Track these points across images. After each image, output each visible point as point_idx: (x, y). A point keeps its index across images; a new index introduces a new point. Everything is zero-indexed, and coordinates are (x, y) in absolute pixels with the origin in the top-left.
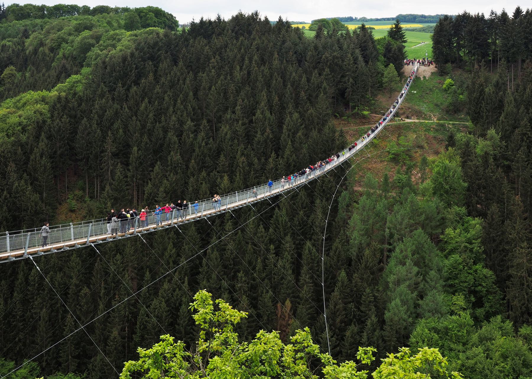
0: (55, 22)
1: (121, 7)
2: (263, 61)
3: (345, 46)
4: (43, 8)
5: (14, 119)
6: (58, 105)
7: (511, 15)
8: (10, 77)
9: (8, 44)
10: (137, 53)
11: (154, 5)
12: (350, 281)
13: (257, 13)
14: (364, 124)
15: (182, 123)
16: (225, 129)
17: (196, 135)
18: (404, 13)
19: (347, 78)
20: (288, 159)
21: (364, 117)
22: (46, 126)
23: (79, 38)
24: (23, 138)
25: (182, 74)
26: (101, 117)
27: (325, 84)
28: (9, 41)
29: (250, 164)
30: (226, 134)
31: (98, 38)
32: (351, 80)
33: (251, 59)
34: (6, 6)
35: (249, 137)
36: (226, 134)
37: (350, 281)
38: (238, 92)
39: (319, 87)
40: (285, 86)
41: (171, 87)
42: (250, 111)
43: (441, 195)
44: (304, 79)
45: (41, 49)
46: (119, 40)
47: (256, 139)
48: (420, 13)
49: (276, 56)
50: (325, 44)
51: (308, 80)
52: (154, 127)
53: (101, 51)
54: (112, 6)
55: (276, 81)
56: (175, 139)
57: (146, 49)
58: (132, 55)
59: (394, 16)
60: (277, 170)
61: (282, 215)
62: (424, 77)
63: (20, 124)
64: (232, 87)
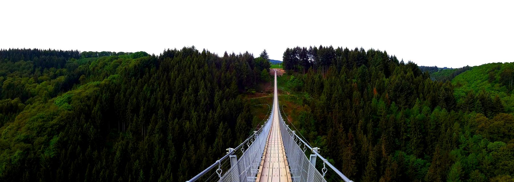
0: (101, 58)
1: (129, 52)
2: (199, 68)
4: (97, 52)
5: (84, 94)
6: (105, 88)
7: (318, 48)
8: (83, 80)
9: (82, 67)
13: (193, 47)
14: (253, 97)
15: (163, 96)
16: (184, 99)
17: (171, 102)
21: (253, 94)
22: (99, 97)
23: (112, 63)
24: (88, 103)
25: (162, 73)
28: (82, 66)
29: (199, 116)
30: (186, 101)
31: (121, 62)
33: (194, 66)
34: (81, 52)
35: (197, 103)
38: (189, 82)
41: (158, 79)
42: (196, 91)
45: (96, 68)
46: (130, 62)
49: (206, 65)
52: (151, 98)
53: (122, 67)
54: (125, 52)
56: (161, 103)
57: (144, 63)
58: (139, 65)
61: (283, 88)
62: (280, 76)
63: (87, 96)
64: (186, 79)
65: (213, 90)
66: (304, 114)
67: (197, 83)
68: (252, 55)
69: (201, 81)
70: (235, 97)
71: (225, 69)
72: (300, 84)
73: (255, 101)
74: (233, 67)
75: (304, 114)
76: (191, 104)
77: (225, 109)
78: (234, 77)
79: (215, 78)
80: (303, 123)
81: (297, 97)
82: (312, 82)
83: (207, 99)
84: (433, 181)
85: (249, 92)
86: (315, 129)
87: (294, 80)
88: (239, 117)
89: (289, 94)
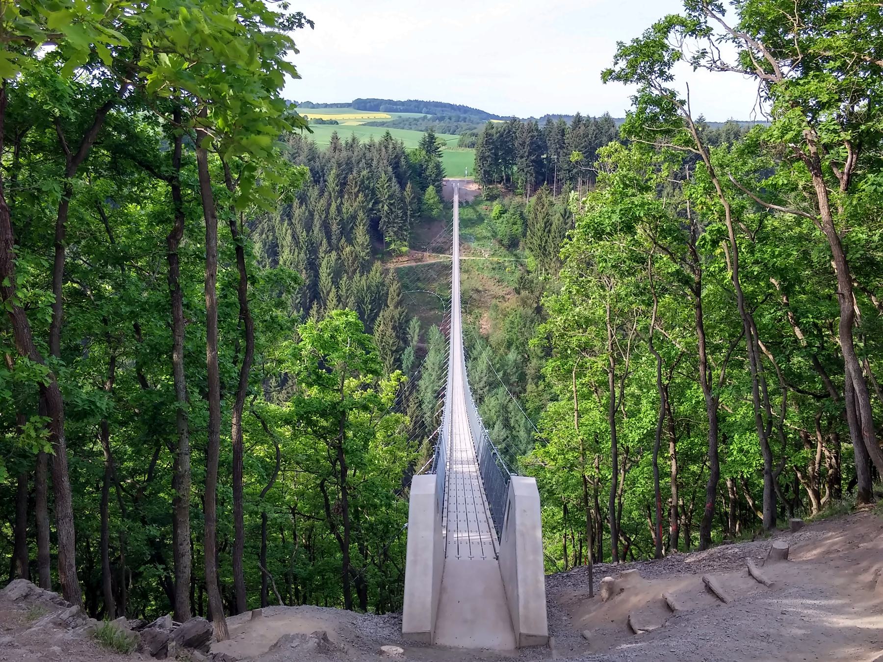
18: (364, 97)
19: (381, 205)
32: (386, 208)
39: (354, 218)
43: (517, 348)
50: (348, 159)
65: (313, 249)
66: (518, 316)
67: (272, 229)
68: (402, 143)
69: (282, 224)
70: (365, 268)
71: (337, 188)
72: (515, 227)
73: (407, 274)
74: (356, 182)
75: (518, 316)
77: (347, 297)
78: (361, 214)
79: (317, 217)
80: (515, 338)
81: (506, 264)
82: (546, 227)
84: (5, 518)
85: (394, 250)
86: (543, 354)
87: (501, 217)
88: (379, 319)
89: (486, 256)
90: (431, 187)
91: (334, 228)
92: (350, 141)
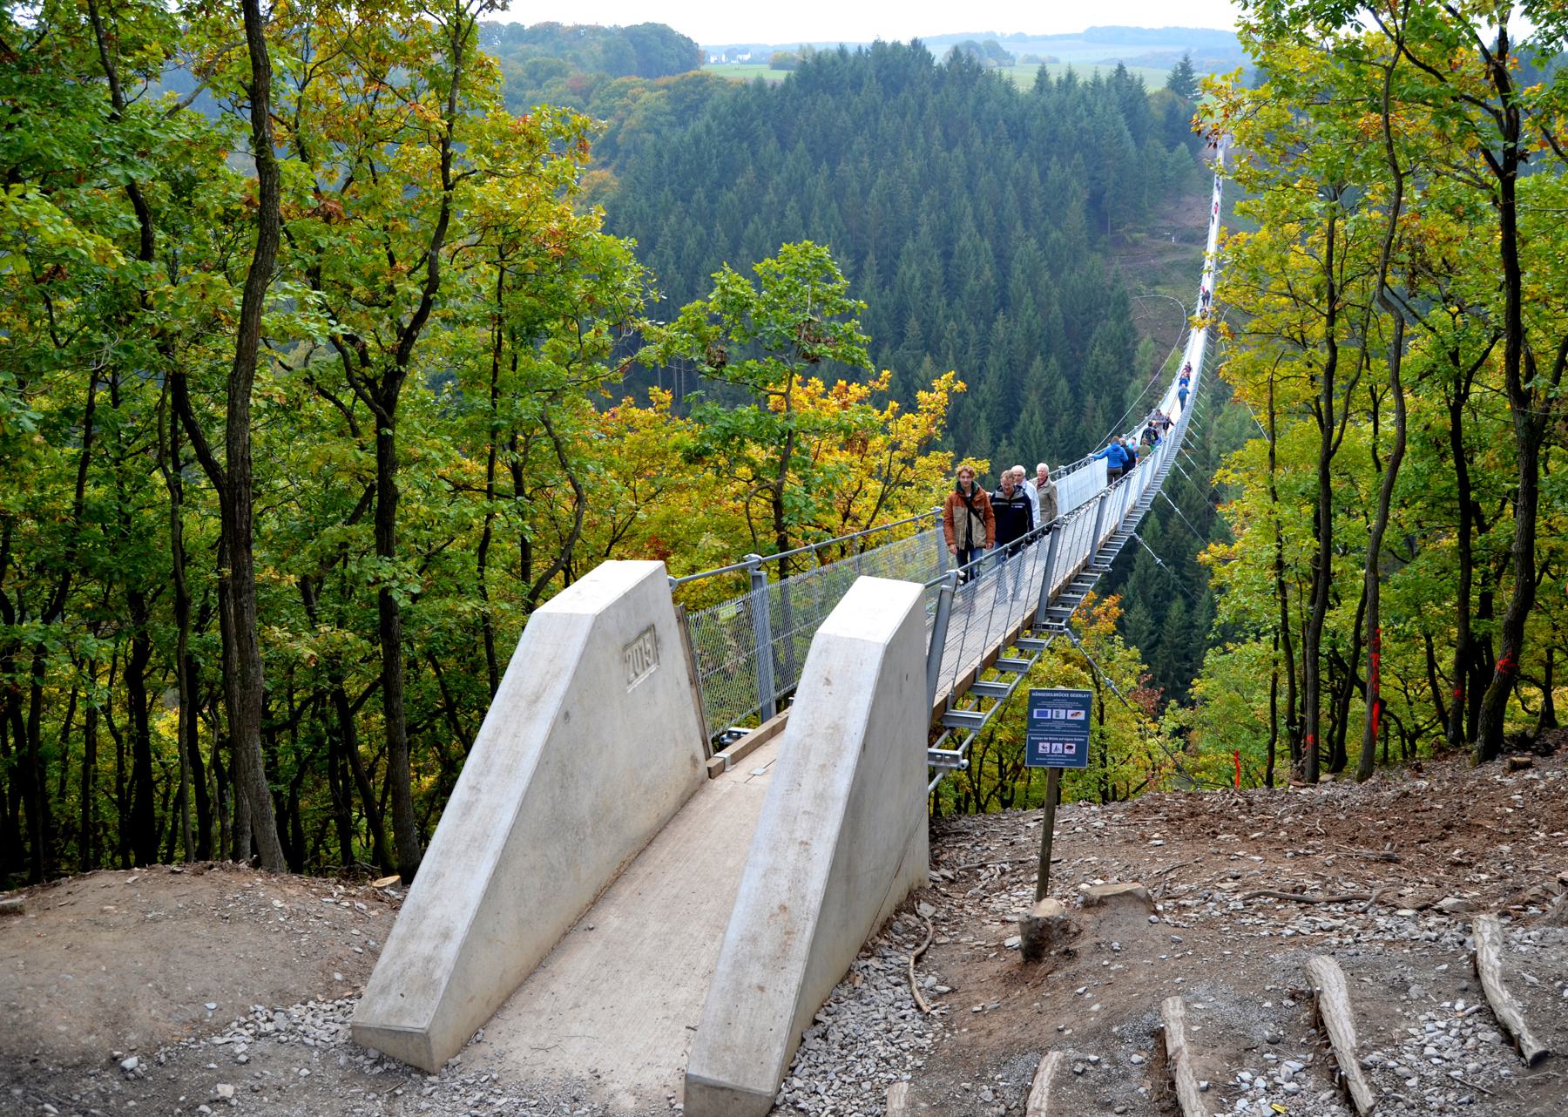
3: (1098, 109)
10: (714, 125)
11: (658, 19)
12: (1165, 531)
20: (1029, 323)
26: (678, 251)
27: (1074, 183)
32: (1113, 175)
36: (913, 278)
37: (1165, 531)
38: (917, 200)
40: (1003, 187)
44: (1035, 175)
47: (968, 287)
48: (1132, 23)
51: (1043, 176)
55: (985, 180)
59: (1081, 31)
60: (1010, 343)
76: (934, 292)
83: (987, 273)
90: (1183, 145)
91: (1035, 203)
92: (1064, 77)
